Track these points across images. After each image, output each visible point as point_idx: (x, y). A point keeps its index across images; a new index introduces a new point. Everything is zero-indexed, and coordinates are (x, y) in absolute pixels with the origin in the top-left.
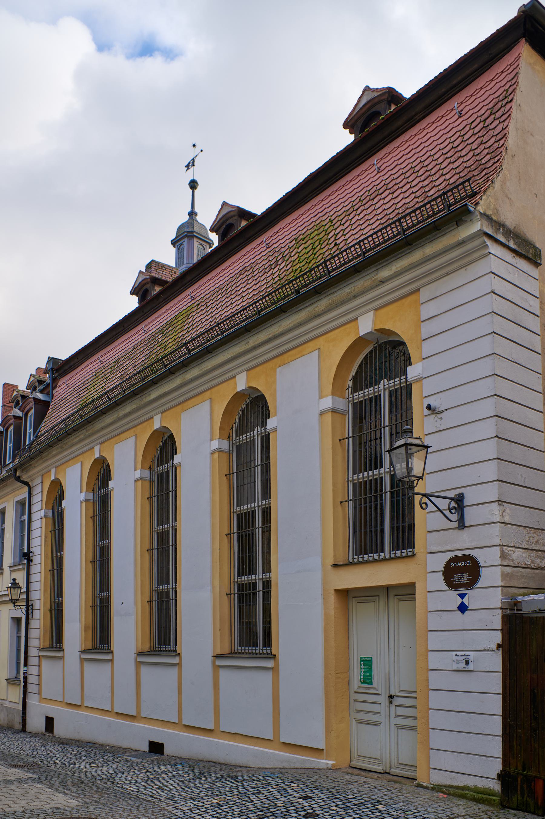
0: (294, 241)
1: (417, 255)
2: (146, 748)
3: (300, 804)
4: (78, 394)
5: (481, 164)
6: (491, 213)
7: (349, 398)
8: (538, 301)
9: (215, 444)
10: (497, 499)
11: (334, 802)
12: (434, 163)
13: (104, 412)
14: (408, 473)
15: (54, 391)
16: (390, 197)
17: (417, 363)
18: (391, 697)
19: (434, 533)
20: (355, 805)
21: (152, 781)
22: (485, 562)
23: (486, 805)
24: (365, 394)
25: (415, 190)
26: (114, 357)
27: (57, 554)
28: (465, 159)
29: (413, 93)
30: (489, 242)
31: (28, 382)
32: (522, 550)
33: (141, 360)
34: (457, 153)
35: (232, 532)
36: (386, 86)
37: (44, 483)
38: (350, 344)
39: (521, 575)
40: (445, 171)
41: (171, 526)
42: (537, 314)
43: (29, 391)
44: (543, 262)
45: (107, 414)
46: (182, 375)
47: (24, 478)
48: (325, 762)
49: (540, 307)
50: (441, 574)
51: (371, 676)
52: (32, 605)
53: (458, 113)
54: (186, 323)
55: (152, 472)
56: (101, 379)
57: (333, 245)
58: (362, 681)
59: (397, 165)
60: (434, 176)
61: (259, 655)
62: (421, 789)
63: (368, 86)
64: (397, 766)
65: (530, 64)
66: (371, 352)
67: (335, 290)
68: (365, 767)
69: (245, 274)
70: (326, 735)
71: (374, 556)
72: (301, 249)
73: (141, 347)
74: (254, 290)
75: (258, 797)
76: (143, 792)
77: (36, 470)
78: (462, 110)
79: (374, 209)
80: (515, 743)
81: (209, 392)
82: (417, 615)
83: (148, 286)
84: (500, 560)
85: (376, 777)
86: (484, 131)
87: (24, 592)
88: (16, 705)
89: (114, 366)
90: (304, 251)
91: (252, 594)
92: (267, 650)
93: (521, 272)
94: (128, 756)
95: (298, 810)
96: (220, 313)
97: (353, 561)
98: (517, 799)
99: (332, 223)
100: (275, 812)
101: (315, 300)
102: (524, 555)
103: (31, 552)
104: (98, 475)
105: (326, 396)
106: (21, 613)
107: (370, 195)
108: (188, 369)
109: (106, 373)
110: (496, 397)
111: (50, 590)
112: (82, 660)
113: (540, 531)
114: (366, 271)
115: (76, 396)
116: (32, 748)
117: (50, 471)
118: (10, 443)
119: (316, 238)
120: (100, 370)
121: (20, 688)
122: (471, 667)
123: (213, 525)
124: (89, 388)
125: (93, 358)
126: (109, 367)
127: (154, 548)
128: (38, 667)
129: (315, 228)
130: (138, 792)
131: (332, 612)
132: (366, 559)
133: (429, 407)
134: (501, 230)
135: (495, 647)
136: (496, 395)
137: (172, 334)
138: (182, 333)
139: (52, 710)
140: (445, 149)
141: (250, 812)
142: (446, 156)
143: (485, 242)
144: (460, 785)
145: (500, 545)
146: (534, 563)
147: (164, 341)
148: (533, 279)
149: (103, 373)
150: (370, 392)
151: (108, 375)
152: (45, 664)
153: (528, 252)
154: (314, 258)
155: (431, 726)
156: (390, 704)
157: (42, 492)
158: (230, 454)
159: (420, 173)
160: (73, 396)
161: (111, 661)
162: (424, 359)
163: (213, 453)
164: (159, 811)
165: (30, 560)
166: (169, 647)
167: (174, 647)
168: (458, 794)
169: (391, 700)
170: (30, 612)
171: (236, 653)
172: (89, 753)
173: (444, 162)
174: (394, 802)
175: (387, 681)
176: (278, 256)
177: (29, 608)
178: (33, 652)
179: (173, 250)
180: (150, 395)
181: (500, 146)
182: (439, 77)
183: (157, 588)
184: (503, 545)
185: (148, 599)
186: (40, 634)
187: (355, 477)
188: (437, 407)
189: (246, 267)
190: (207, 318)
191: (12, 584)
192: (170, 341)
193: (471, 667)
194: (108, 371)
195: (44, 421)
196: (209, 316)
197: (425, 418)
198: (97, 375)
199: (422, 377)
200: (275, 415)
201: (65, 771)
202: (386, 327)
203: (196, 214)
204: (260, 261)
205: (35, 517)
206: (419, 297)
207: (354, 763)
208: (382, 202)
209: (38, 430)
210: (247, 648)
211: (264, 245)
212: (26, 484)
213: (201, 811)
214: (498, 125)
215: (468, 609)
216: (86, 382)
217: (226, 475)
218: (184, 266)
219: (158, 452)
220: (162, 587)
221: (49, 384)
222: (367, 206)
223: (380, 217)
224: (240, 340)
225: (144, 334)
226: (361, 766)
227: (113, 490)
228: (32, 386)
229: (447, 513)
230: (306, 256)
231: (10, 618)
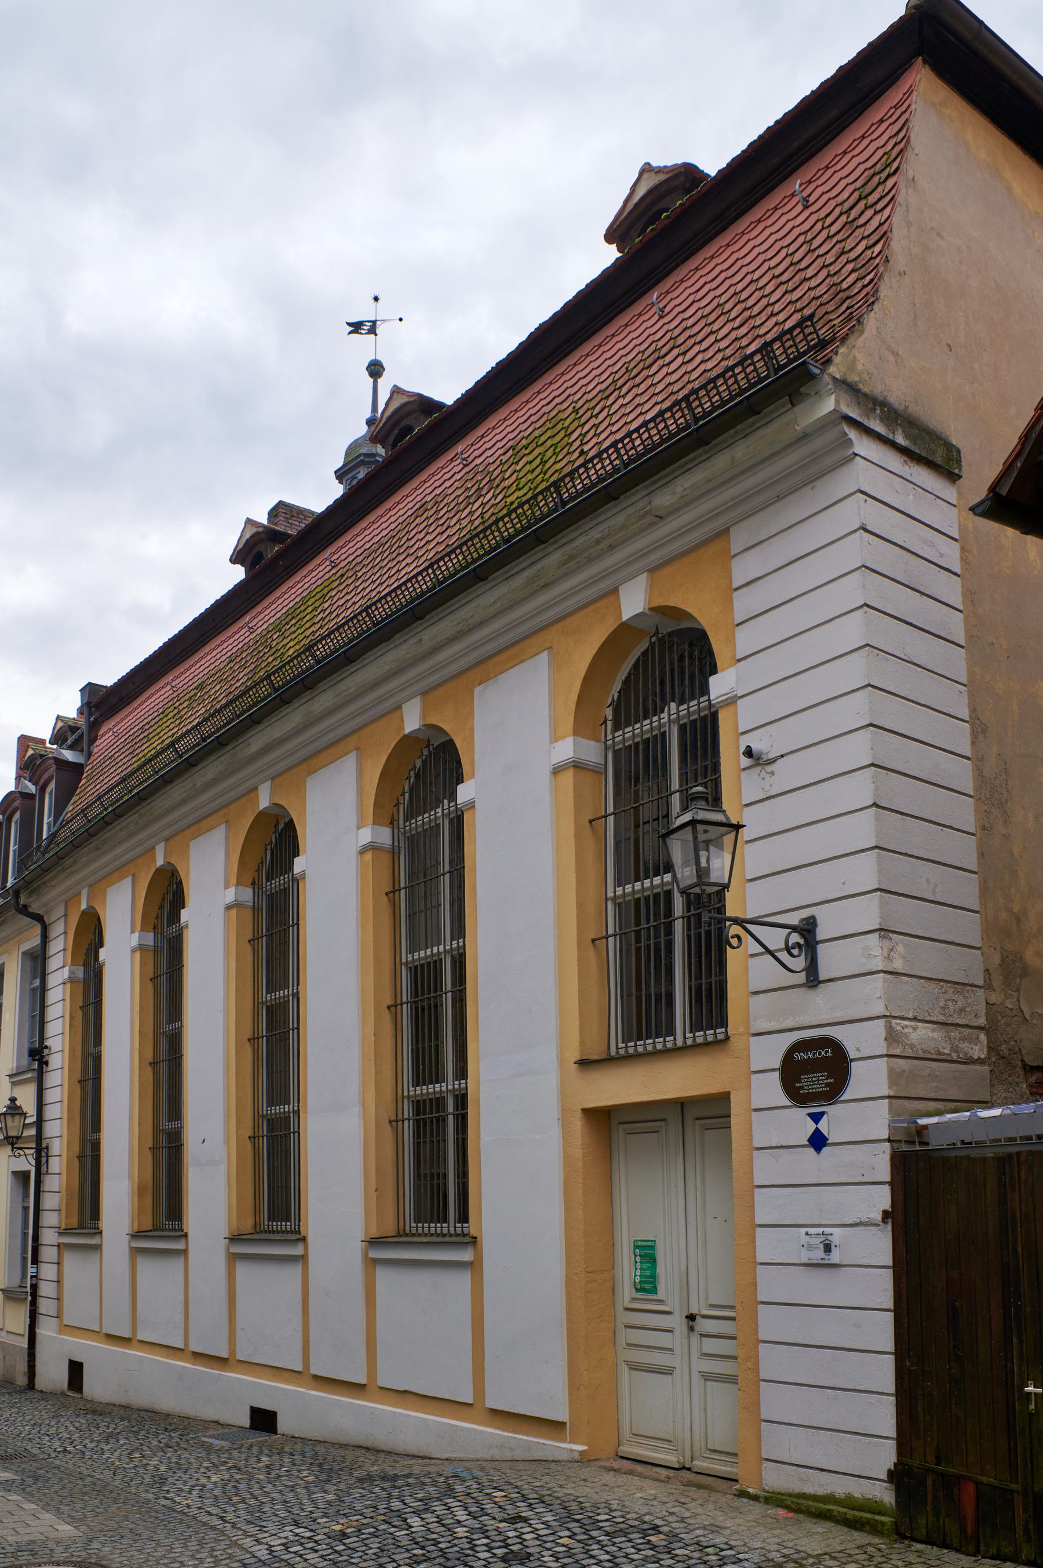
0: (511, 451)
1: (720, 462)
3: (500, 1533)
4: (132, 749)
5: (840, 291)
6: (856, 379)
7: (606, 741)
8: (957, 545)
9: (366, 836)
10: (878, 927)
11: (568, 1529)
12: (758, 295)
13: (167, 780)
14: (699, 877)
16: (680, 360)
17: (728, 668)
18: (691, 1318)
19: (762, 996)
20: (607, 1534)
21: (235, 1487)
22: (858, 1049)
23: (868, 1533)
24: (636, 732)
25: (723, 345)
26: (196, 678)
27: (92, 1049)
28: (813, 283)
29: (721, 168)
30: (852, 434)
32: (931, 1026)
33: (241, 682)
34: (800, 273)
35: (399, 1001)
36: (680, 161)
38: (606, 636)
39: (930, 1075)
40: (777, 308)
41: (290, 992)
42: (954, 570)
43: (55, 746)
44: (965, 472)
45: (174, 784)
46: (304, 706)
47: (35, 908)
49: (961, 558)
50: (776, 1075)
51: (654, 1277)
52: (47, 1148)
53: (801, 200)
54: (319, 610)
55: (256, 890)
56: (172, 720)
57: (577, 454)
58: (638, 1287)
59: (694, 302)
60: (758, 318)
61: (447, 1239)
62: (745, 1500)
63: (649, 164)
64: (705, 1455)
65: (934, 104)
66: (645, 653)
68: (646, 1456)
69: (425, 516)
70: (569, 1394)
71: (654, 1043)
72: (521, 464)
73: (242, 659)
74: (438, 543)
75: (422, 1519)
76: (208, 1509)
77: (54, 893)
78: (809, 195)
79: (652, 384)
80: (920, 1409)
81: (355, 737)
82: (733, 1156)
84: (885, 1046)
85: (662, 1478)
86: (847, 230)
88: (19, 1338)
89: (195, 695)
90: (528, 468)
91: (434, 1120)
92: (462, 1227)
93: (920, 490)
94: (210, 1437)
95: (493, 1544)
96: (377, 590)
97: (618, 1052)
98: (927, 1521)
99: (577, 413)
100: (447, 1551)
101: (539, 555)
102: (935, 1035)
103: (46, 1047)
104: (163, 899)
105: (564, 737)
106: (26, 1163)
107: (645, 359)
108: (314, 694)
109: (181, 708)
110: (871, 728)
111: (79, 1118)
112: (135, 1252)
113: (970, 988)
114: (629, 497)
115: (128, 752)
116: (32, 1422)
119: (549, 443)
120: (171, 703)
122: (835, 1257)
124: (150, 736)
125: (161, 683)
126: (187, 697)
127: (260, 1034)
128: (56, 1266)
129: (549, 425)
130: (200, 1508)
131: (578, 1153)
132: (640, 1049)
133: (749, 753)
134: (878, 412)
135: (879, 1217)
136: (871, 725)
137: (295, 632)
138: (313, 629)
139: (83, 1348)
140: (779, 267)
141: (399, 1550)
142: (779, 280)
143: (846, 434)
144: (818, 1493)
145: (884, 1016)
146: (957, 1052)
147: (282, 644)
148: (946, 504)
149: (175, 708)
150: (645, 727)
151: (183, 713)
152: (69, 1259)
153: (934, 454)
154: (543, 481)
155: (762, 1376)
156: (691, 1333)
157: (65, 933)
158: (394, 852)
159: (733, 314)
160: (123, 753)
161: (184, 1252)
162: (739, 661)
163: (363, 851)
164: (225, 1547)
165: (43, 1063)
166: (288, 1223)
168: (814, 1510)
169: (691, 1323)
170: (44, 1160)
171: (407, 1235)
172: (136, 1432)
173: (776, 292)
174: (685, 1528)
175: (685, 1288)
176: (483, 479)
177: (41, 1153)
178: (48, 1237)
180: (249, 745)
181: (874, 255)
182: (766, 136)
183: (267, 1111)
184: (891, 1016)
185: (250, 1133)
186: (60, 1203)
187: (619, 891)
188: (764, 752)
189: (426, 502)
190: (356, 599)
192: (291, 644)
193: (835, 1257)
194: (185, 705)
195: (72, 801)
196: (360, 596)
197: (743, 774)
198: (165, 713)
199: (736, 696)
200: (473, 776)
201: (79, 1467)
202: (671, 603)
204: (450, 491)
206: (730, 543)
207: (626, 1449)
208: (665, 370)
210: (426, 1225)
211: (459, 461)
212: (38, 918)
213: (305, 1549)
214: (871, 218)
215: (829, 1142)
216: (147, 727)
217: (387, 894)
220: (275, 1109)
221: (81, 736)
222: (638, 380)
223: (660, 398)
224: (406, 637)
225: (248, 633)
226: (638, 1455)
227: (187, 926)
228: (59, 737)
229: (783, 956)
230: (530, 477)
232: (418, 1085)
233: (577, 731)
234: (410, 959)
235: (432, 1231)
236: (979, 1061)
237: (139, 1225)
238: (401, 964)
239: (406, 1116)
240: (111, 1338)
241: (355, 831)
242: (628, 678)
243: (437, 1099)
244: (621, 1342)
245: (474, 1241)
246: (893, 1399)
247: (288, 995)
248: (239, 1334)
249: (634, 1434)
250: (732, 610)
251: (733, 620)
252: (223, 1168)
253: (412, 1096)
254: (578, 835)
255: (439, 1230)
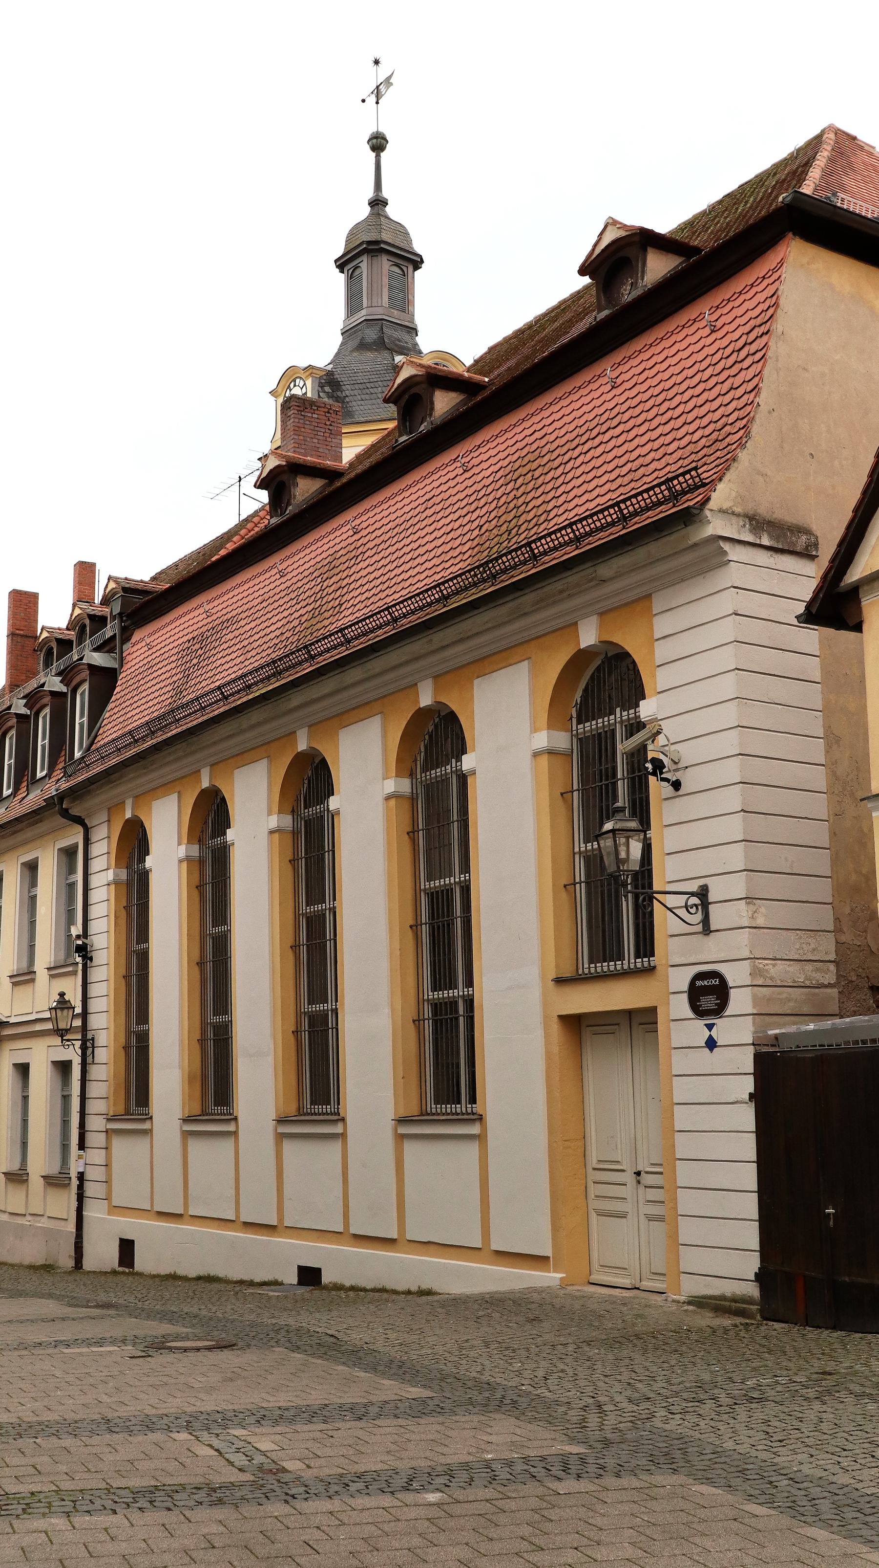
2: (292, 1278)
9: (390, 786)
15: (125, 647)
18: (638, 1174)
27: (137, 947)
31: (71, 618)
32: (788, 963)
37: (112, 822)
46: (337, 677)
47: (75, 811)
48: (551, 1278)
52: (93, 1039)
55: (295, 817)
61: (460, 1117)
67: (543, 584)
77: (97, 800)
83: (284, 477)
87: (78, 1015)
106: (73, 1054)
117: (124, 802)
118: (44, 738)
121: (70, 1191)
123: (390, 911)
127: (301, 943)
128: (104, 1150)
131: (556, 1049)
152: (118, 1144)
157: (109, 837)
161: (235, 1134)
162: (659, 693)
167: (336, 1107)
169: (638, 1178)
170: (89, 1051)
171: (428, 1114)
177: (87, 1046)
178: (95, 1123)
179: (340, 279)
180: (290, 699)
183: (308, 1008)
184: (755, 958)
185: (293, 1028)
191: (59, 1002)
195: (108, 708)
203: (385, 203)
205: (96, 881)
209: (98, 725)
210: (444, 1106)
212: (80, 821)
217: (408, 833)
218: (364, 312)
219: (306, 786)
220: (312, 1008)
227: (233, 844)
229: (682, 913)
231: (50, 1063)
232: (436, 991)
233: (551, 726)
234: (427, 887)
235: (449, 1111)
236: (829, 986)
237: (189, 1111)
238: (420, 890)
239: (426, 1017)
240: (162, 1215)
241: (381, 781)
242: (593, 674)
243: (451, 1002)
244: (591, 1195)
245: (480, 1118)
246: (757, 1223)
247: (326, 909)
248: (287, 1204)
249: (601, 1266)
250: (654, 654)
251: (654, 663)
252: (270, 1059)
253: (431, 1000)
254: (552, 806)
255: (454, 1110)
